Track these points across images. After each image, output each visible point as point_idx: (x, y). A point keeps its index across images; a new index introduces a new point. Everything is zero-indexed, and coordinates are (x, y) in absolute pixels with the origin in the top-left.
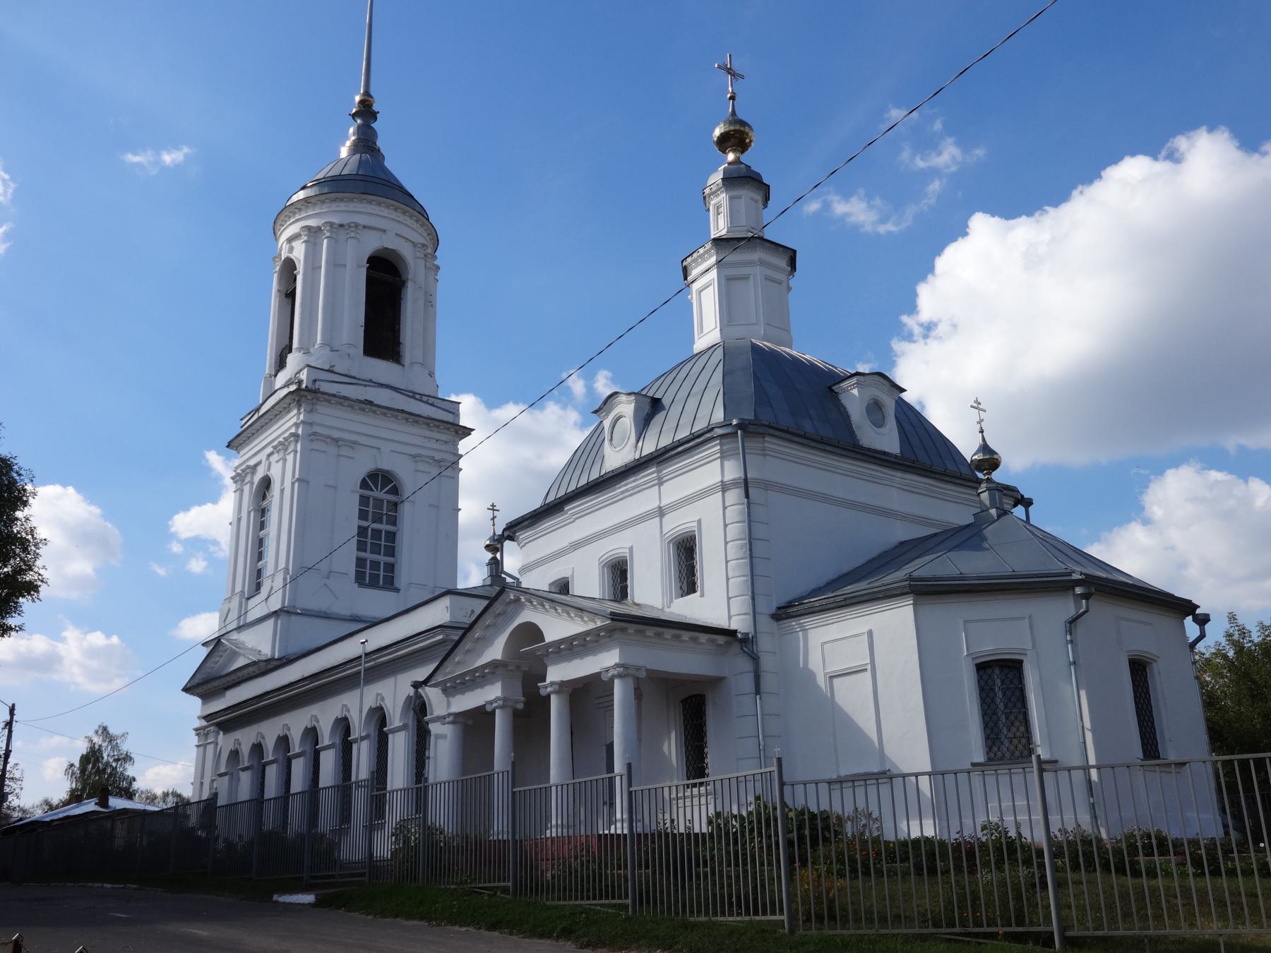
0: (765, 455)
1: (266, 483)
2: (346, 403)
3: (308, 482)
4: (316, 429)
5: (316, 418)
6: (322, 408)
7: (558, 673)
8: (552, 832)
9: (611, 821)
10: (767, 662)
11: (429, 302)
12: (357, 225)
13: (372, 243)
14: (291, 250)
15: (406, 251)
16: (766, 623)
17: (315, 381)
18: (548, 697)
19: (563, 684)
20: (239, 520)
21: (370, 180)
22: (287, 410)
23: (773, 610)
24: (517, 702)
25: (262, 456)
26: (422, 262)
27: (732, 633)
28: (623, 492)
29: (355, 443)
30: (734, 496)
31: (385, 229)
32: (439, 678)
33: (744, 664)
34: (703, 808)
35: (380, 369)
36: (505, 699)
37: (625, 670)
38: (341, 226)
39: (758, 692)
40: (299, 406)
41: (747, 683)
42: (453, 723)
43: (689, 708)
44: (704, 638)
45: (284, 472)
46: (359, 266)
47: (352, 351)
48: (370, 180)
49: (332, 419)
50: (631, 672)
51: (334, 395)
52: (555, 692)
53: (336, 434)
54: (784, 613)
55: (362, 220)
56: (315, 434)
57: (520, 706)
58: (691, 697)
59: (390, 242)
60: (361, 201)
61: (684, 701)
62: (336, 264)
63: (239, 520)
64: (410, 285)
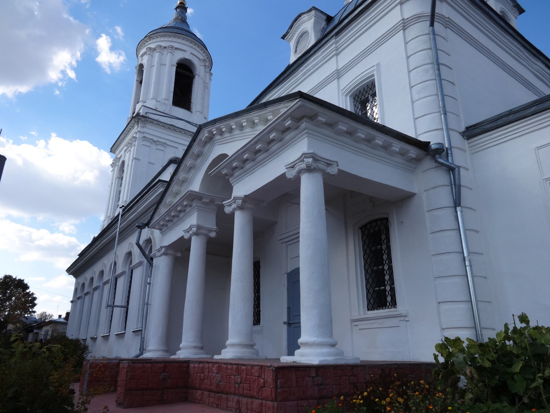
0: (148, 304)
1: (123, 162)
2: (161, 125)
3: (139, 160)
4: (145, 135)
5: (145, 130)
6: (148, 126)
7: (243, 187)
8: (227, 354)
9: (293, 346)
10: (465, 177)
11: (206, 87)
12: (172, 47)
13: (179, 56)
14: (142, 60)
15: (195, 61)
16: (458, 140)
17: (146, 113)
18: (232, 215)
19: (247, 199)
20: (112, 183)
21: (180, 28)
22: (133, 127)
23: (463, 129)
24: (210, 231)
25: (123, 152)
26: (203, 68)
27: (424, 146)
28: (305, 74)
29: (165, 144)
30: (424, 26)
31: (188, 52)
32: (156, 218)
33: (440, 178)
34: (119, 300)
35: (179, 112)
36: (199, 227)
37: (314, 164)
38: (165, 47)
39: (457, 203)
40: (138, 124)
41: (444, 197)
42: (165, 254)
43: (370, 226)
44: (397, 146)
45: (128, 158)
46: (172, 65)
47: (166, 102)
48: (180, 28)
49: (152, 131)
50: (321, 166)
51: (155, 120)
52: (240, 208)
53: (155, 139)
54: (472, 132)
55: (175, 45)
56: (144, 137)
57: (213, 235)
58: (370, 223)
59: (188, 56)
60: (174, 37)
61: (363, 228)
62: (162, 64)
63: (112, 183)
64: (196, 77)
